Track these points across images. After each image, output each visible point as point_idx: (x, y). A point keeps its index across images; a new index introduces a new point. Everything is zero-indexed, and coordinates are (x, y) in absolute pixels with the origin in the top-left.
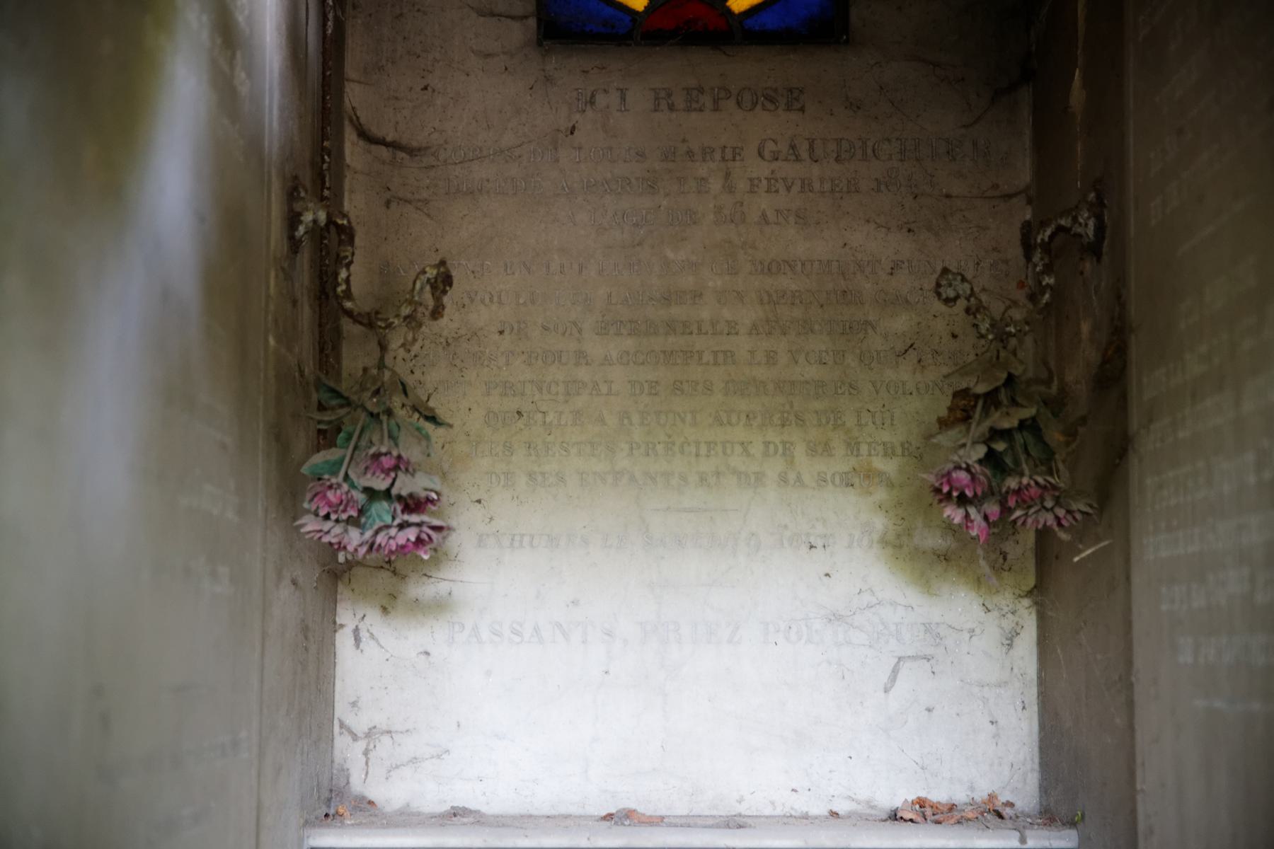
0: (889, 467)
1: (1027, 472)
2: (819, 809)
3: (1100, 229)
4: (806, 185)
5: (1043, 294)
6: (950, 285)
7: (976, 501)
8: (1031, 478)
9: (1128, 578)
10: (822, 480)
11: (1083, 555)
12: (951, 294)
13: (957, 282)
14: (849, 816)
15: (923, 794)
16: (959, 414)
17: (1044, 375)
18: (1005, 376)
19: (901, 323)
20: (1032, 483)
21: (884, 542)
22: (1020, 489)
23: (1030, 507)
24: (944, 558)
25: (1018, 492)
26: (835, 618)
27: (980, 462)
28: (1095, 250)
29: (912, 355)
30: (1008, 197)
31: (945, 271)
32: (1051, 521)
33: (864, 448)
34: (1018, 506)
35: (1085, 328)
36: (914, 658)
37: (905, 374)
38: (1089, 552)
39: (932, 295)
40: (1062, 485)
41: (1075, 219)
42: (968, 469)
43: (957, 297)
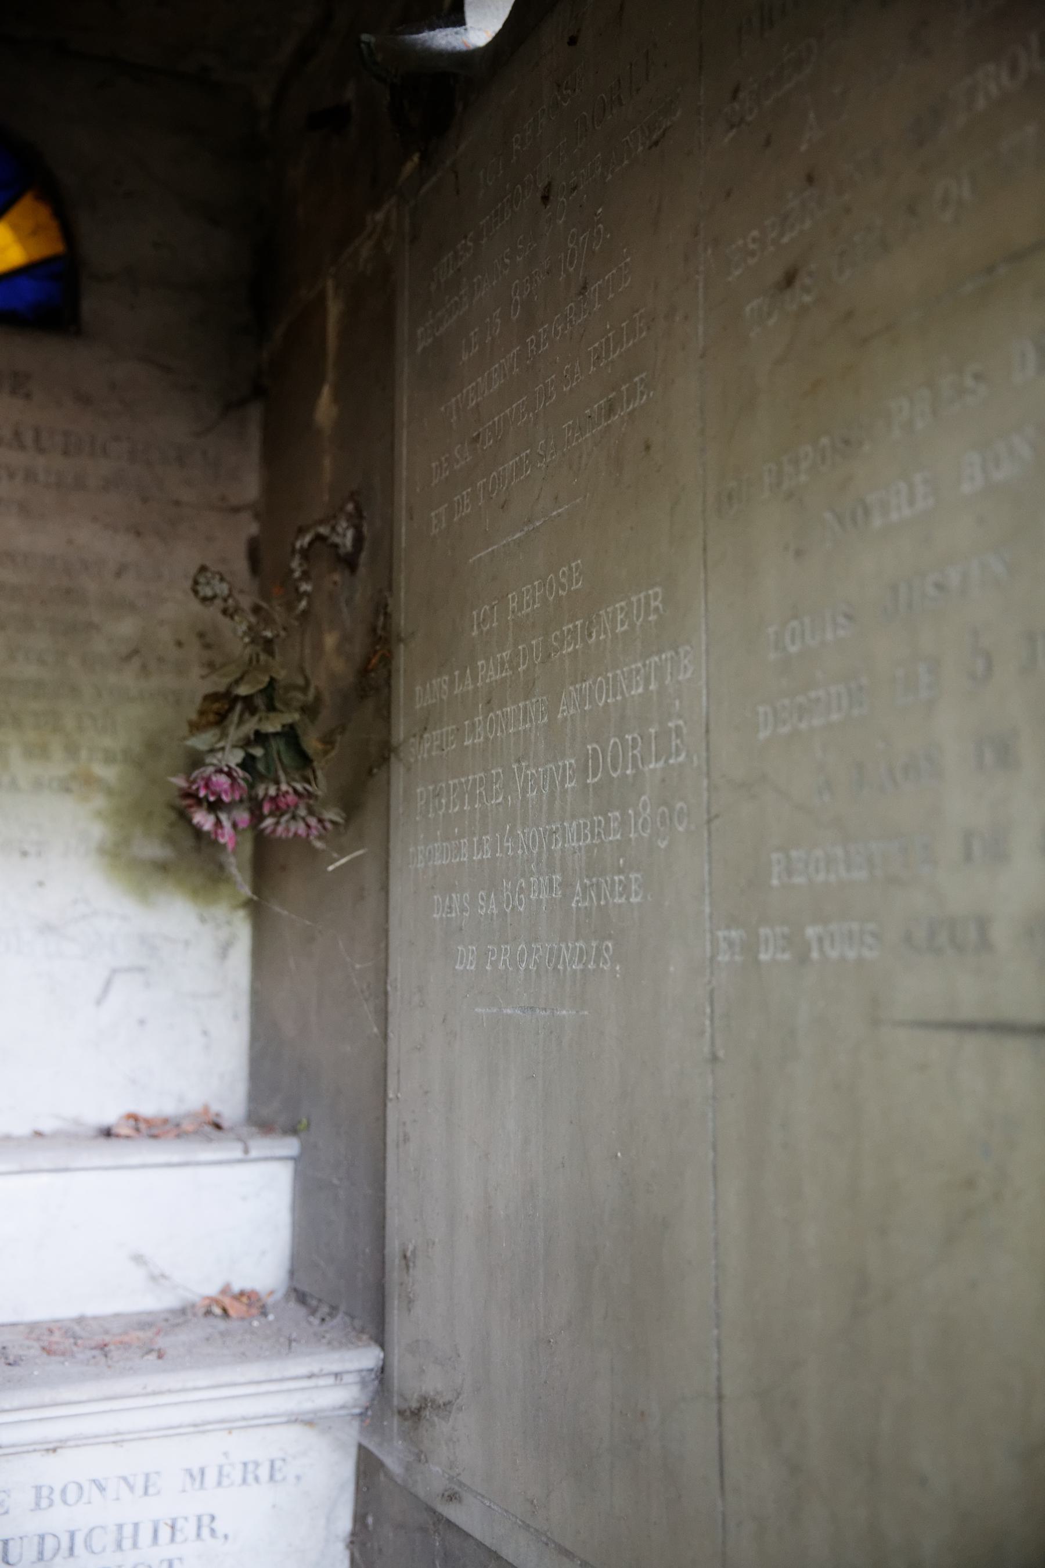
0: (109, 773)
1: (282, 777)
2: (22, 1129)
3: (359, 540)
4: (30, 476)
5: (300, 600)
6: (208, 583)
7: (228, 807)
8: (289, 784)
9: (385, 889)
10: (38, 785)
11: (338, 864)
12: (208, 592)
13: (216, 582)
14: (55, 1135)
15: (132, 1108)
16: (212, 717)
17: (301, 681)
18: (267, 679)
19: (127, 627)
20: (291, 790)
21: (102, 851)
22: (277, 795)
23: (282, 815)
24: (162, 868)
25: (273, 799)
26: (47, 929)
27: (238, 765)
28: (350, 563)
29: (136, 662)
30: (236, 510)
31: (203, 569)
32: (302, 829)
33: (84, 754)
34: (271, 814)
35: (330, 641)
36: (129, 970)
37: (128, 678)
38: (343, 861)
39: (192, 595)
40: (319, 793)
41: (333, 529)
42: (229, 774)
43: (215, 597)
